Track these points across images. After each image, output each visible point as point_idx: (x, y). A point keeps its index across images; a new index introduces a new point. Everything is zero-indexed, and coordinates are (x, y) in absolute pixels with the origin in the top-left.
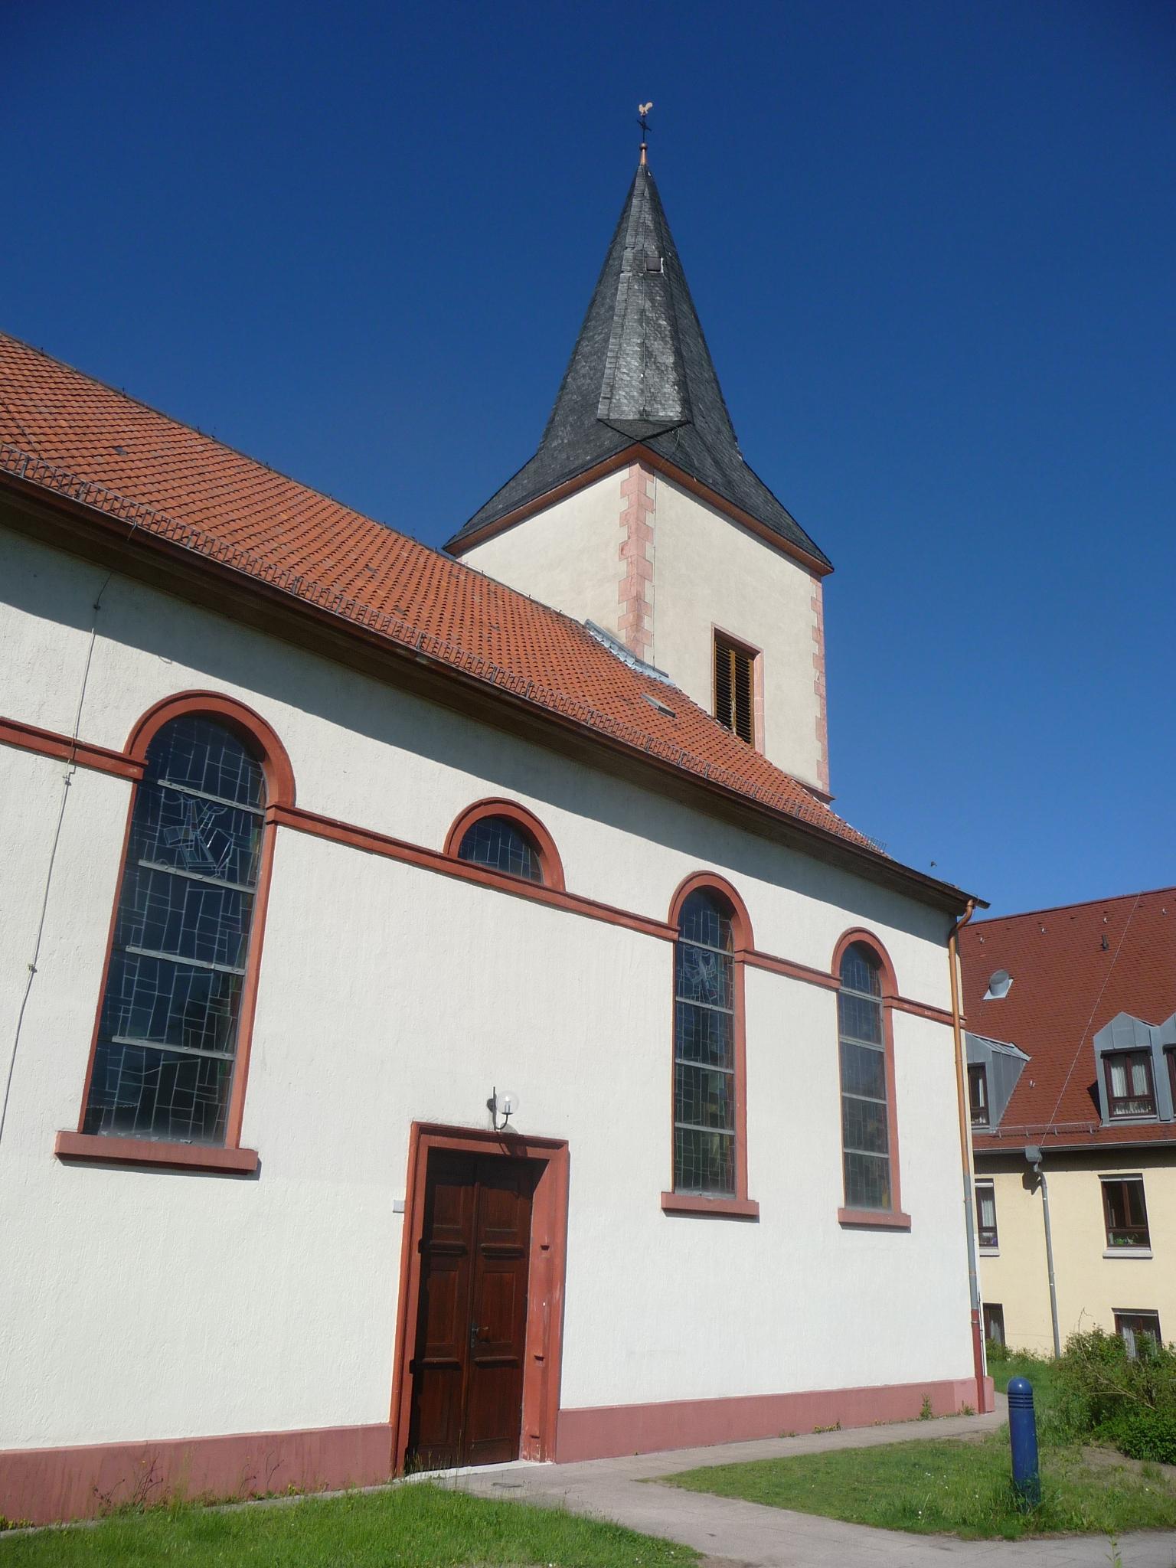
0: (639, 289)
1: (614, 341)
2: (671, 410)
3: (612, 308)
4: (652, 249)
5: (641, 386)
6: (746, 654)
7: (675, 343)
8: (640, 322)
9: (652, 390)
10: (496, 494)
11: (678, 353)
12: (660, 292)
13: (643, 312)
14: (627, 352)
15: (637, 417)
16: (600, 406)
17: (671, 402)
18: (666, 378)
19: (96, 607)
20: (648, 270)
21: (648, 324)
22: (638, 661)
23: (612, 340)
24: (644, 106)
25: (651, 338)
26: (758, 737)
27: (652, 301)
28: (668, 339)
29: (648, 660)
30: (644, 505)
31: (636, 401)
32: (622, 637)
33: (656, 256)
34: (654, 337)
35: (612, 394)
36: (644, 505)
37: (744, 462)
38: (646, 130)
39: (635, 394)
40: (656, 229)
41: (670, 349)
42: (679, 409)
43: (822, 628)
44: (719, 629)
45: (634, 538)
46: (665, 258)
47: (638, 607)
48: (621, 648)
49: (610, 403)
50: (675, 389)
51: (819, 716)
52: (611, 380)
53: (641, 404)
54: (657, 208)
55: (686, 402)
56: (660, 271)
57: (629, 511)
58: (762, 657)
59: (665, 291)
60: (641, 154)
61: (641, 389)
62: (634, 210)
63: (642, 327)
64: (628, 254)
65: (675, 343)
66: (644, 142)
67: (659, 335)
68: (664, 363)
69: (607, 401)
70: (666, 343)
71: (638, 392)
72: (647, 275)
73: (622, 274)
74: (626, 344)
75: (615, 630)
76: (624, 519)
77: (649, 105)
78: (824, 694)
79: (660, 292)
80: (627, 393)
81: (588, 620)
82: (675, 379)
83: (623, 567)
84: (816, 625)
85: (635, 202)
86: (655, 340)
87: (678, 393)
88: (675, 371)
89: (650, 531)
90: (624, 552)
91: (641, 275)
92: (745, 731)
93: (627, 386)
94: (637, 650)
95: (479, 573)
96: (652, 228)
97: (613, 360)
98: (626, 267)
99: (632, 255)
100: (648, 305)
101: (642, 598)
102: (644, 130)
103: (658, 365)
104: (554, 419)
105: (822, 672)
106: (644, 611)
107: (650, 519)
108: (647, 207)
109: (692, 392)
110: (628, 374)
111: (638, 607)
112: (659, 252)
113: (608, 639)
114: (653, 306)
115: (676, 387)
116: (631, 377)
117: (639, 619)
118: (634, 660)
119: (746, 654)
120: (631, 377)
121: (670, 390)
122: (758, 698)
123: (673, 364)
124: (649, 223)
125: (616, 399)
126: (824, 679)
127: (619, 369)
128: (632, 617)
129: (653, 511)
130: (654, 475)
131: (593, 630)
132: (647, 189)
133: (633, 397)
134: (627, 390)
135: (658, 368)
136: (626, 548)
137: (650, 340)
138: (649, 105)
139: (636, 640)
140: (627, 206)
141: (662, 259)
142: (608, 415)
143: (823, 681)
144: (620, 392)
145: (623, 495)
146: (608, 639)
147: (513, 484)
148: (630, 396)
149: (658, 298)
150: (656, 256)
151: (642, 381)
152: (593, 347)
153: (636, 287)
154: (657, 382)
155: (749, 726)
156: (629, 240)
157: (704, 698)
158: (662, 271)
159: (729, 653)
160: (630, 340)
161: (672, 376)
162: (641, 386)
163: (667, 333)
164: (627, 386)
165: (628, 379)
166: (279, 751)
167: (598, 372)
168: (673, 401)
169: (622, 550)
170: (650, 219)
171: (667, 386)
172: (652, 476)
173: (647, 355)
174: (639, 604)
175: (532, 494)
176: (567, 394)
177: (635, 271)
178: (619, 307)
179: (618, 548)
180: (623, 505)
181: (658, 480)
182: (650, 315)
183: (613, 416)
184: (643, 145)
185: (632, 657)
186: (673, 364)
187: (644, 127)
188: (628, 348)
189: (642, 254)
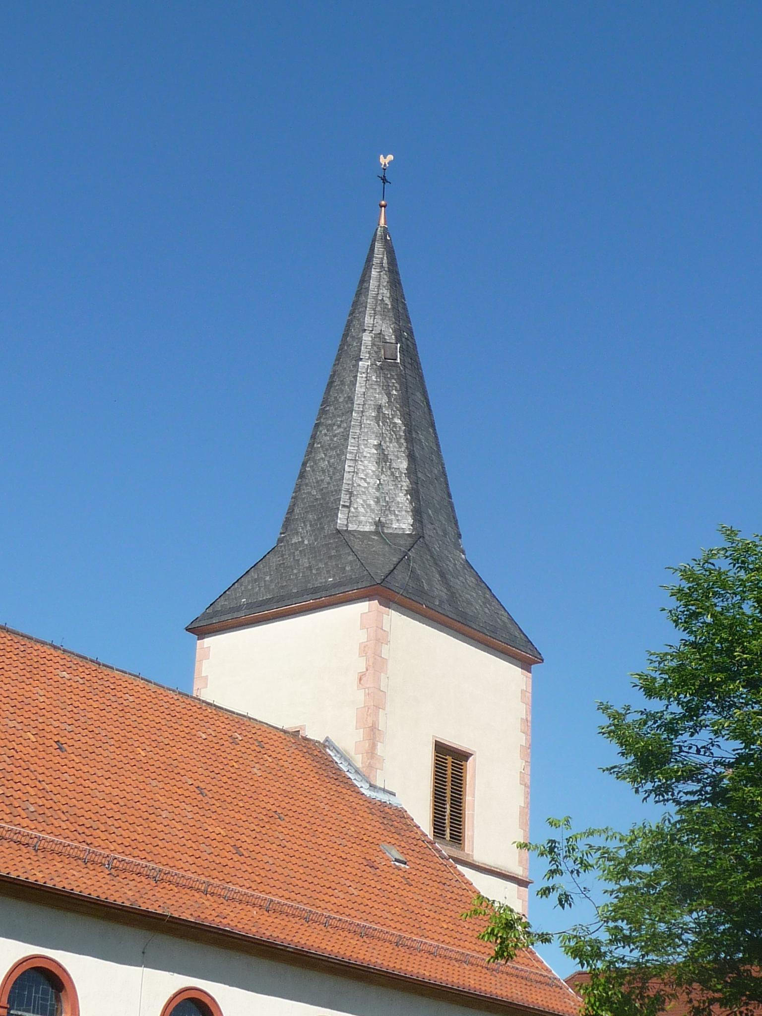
0: (377, 381)
1: (353, 441)
2: (404, 524)
3: (350, 400)
4: (389, 334)
5: (378, 494)
6: (462, 757)
7: (409, 447)
8: (377, 419)
9: (387, 499)
10: (238, 580)
11: (411, 457)
12: (396, 385)
13: (379, 408)
14: (365, 454)
15: (373, 528)
16: (339, 515)
17: (404, 513)
18: (400, 486)
19: (143, 953)
20: (385, 359)
21: (384, 422)
22: (372, 787)
23: (351, 440)
24: (385, 158)
25: (387, 439)
26: (468, 835)
27: (389, 395)
28: (402, 441)
29: (380, 784)
30: (380, 638)
31: (372, 511)
32: (359, 761)
33: (393, 341)
34: (390, 438)
35: (351, 501)
36: (380, 638)
37: (467, 560)
38: (387, 184)
39: (372, 502)
40: (393, 308)
41: (404, 452)
42: (411, 521)
43: (529, 719)
44: (439, 740)
45: (371, 671)
46: (402, 343)
47: (373, 733)
48: (357, 772)
49: (349, 512)
50: (407, 499)
51: (523, 806)
52: (350, 487)
53: (377, 514)
54: (395, 283)
55: (417, 513)
56: (396, 360)
57: (368, 643)
58: (474, 760)
59: (401, 384)
60: (381, 211)
61: (377, 498)
62: (373, 284)
63: (379, 425)
64: (367, 338)
65: (409, 447)
66: (383, 200)
67: (394, 436)
68: (399, 469)
69: (346, 510)
70: (400, 446)
71: (374, 501)
72: (384, 367)
73: (360, 363)
74: (364, 445)
75: (352, 753)
76: (363, 650)
77: (390, 157)
78: (529, 783)
79: (396, 385)
80: (364, 501)
81: (328, 737)
82: (408, 486)
83: (360, 696)
84: (524, 717)
85: (374, 273)
86: (391, 442)
87: (411, 503)
88: (409, 478)
89: (384, 661)
90: (362, 682)
91: (379, 363)
92: (457, 838)
93: (364, 493)
94: (371, 776)
95: (244, 716)
96: (390, 307)
97: (351, 463)
98: (364, 354)
99: (370, 339)
100: (384, 400)
101: (377, 727)
102: (384, 183)
103: (393, 470)
104: (293, 510)
105: (526, 762)
106: (377, 739)
107: (385, 651)
108: (385, 278)
109: (423, 499)
110: (365, 480)
111: (373, 733)
112: (396, 337)
113: (346, 760)
114: (390, 401)
115: (409, 497)
116: (368, 483)
117: (373, 746)
118: (368, 785)
119: (462, 757)
120: (368, 483)
121: (403, 499)
122: (470, 798)
123: (407, 469)
124: (387, 301)
125: (354, 508)
126: (529, 768)
127: (357, 473)
128: (367, 745)
129: (388, 643)
130: (389, 608)
131: (332, 748)
132: (385, 258)
133: (369, 506)
134: (364, 497)
135: (392, 474)
136: (364, 679)
137: (385, 442)
138: (390, 157)
139: (370, 766)
140: (365, 278)
141: (399, 345)
142: (347, 526)
143: (528, 770)
144: (358, 500)
145: (363, 627)
146: (346, 760)
147: (254, 575)
148: (367, 505)
149: (394, 392)
150: (393, 341)
151: (378, 488)
152: (332, 440)
153: (374, 378)
154: (391, 489)
155: (461, 803)
156: (368, 320)
157: (423, 819)
158: (399, 361)
159: (446, 760)
160: (367, 440)
161: (405, 483)
162: (378, 494)
163: (402, 434)
164: (364, 493)
165: (366, 485)
166: (219, 1013)
167: (337, 472)
168: (406, 511)
169: (360, 680)
170: (388, 295)
171: (400, 494)
172: (388, 609)
173: (383, 458)
174: (374, 734)
175: (280, 599)
176: (307, 485)
177: (373, 360)
178: (358, 401)
179: (356, 677)
180: (362, 637)
181: (393, 611)
182: (386, 412)
183: (352, 527)
184: (383, 203)
185: (367, 782)
186: (407, 469)
187: (384, 180)
188: (366, 449)
189: (380, 338)
